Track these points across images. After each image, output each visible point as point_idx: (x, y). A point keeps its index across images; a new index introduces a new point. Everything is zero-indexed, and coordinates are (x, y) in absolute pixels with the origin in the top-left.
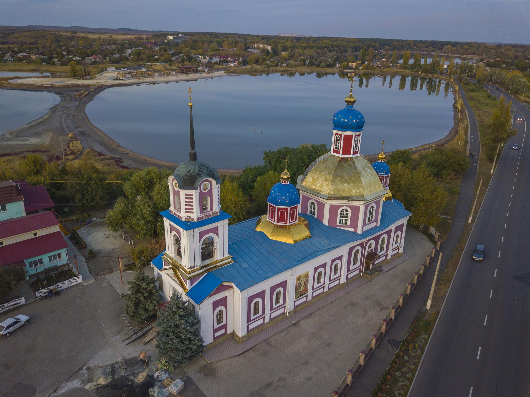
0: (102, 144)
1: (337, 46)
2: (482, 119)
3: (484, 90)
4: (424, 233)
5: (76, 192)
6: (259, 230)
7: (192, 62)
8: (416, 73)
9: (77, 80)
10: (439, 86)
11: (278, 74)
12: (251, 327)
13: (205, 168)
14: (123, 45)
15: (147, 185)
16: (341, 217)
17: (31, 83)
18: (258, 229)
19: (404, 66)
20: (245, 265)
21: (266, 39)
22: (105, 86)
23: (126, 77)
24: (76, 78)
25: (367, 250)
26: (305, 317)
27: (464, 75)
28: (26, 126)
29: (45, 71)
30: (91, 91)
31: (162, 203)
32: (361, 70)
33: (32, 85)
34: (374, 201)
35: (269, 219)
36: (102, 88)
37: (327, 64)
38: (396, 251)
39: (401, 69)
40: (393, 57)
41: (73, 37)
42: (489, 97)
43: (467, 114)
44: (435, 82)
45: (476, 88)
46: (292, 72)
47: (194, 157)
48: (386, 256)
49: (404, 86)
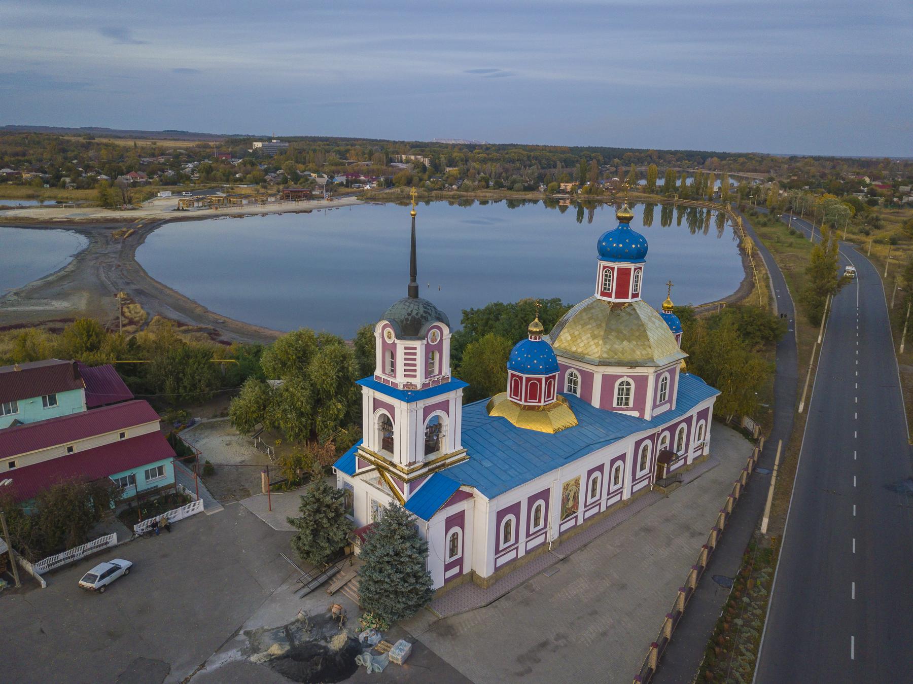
0: (178, 308)
1: (536, 158)
2: (787, 265)
3: (783, 223)
4: (733, 428)
5: (166, 376)
6: (497, 415)
7: (301, 183)
8: (670, 199)
9: (109, 211)
10: (708, 220)
11: (445, 203)
12: (502, 561)
13: (433, 310)
14: (177, 156)
15: (299, 355)
16: (619, 394)
17: (30, 217)
18: (494, 413)
19: (650, 188)
20: (487, 464)
21: (419, 147)
22: (160, 220)
23: (193, 206)
24: (108, 209)
25: (659, 449)
26: (579, 549)
27: (747, 201)
28: (39, 283)
29: (50, 198)
30: (139, 228)
31: (327, 383)
32: (580, 194)
33: (33, 219)
34: (667, 369)
35: (511, 397)
36: (154, 224)
37: (524, 186)
38: (699, 453)
39: (644, 193)
40: (629, 175)
41: (89, 143)
42: (793, 233)
43: (763, 258)
44: (701, 213)
45: (770, 220)
46: (469, 198)
47: (414, 292)
48: (686, 458)
49: (652, 219)
